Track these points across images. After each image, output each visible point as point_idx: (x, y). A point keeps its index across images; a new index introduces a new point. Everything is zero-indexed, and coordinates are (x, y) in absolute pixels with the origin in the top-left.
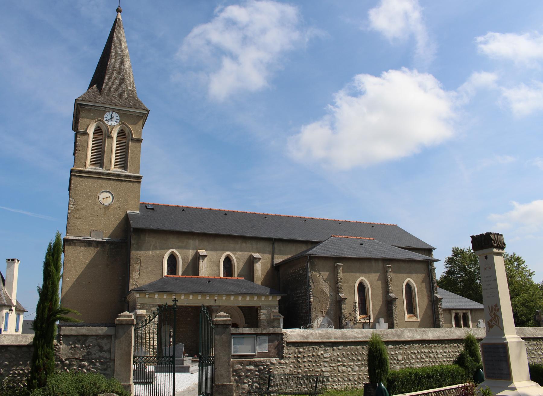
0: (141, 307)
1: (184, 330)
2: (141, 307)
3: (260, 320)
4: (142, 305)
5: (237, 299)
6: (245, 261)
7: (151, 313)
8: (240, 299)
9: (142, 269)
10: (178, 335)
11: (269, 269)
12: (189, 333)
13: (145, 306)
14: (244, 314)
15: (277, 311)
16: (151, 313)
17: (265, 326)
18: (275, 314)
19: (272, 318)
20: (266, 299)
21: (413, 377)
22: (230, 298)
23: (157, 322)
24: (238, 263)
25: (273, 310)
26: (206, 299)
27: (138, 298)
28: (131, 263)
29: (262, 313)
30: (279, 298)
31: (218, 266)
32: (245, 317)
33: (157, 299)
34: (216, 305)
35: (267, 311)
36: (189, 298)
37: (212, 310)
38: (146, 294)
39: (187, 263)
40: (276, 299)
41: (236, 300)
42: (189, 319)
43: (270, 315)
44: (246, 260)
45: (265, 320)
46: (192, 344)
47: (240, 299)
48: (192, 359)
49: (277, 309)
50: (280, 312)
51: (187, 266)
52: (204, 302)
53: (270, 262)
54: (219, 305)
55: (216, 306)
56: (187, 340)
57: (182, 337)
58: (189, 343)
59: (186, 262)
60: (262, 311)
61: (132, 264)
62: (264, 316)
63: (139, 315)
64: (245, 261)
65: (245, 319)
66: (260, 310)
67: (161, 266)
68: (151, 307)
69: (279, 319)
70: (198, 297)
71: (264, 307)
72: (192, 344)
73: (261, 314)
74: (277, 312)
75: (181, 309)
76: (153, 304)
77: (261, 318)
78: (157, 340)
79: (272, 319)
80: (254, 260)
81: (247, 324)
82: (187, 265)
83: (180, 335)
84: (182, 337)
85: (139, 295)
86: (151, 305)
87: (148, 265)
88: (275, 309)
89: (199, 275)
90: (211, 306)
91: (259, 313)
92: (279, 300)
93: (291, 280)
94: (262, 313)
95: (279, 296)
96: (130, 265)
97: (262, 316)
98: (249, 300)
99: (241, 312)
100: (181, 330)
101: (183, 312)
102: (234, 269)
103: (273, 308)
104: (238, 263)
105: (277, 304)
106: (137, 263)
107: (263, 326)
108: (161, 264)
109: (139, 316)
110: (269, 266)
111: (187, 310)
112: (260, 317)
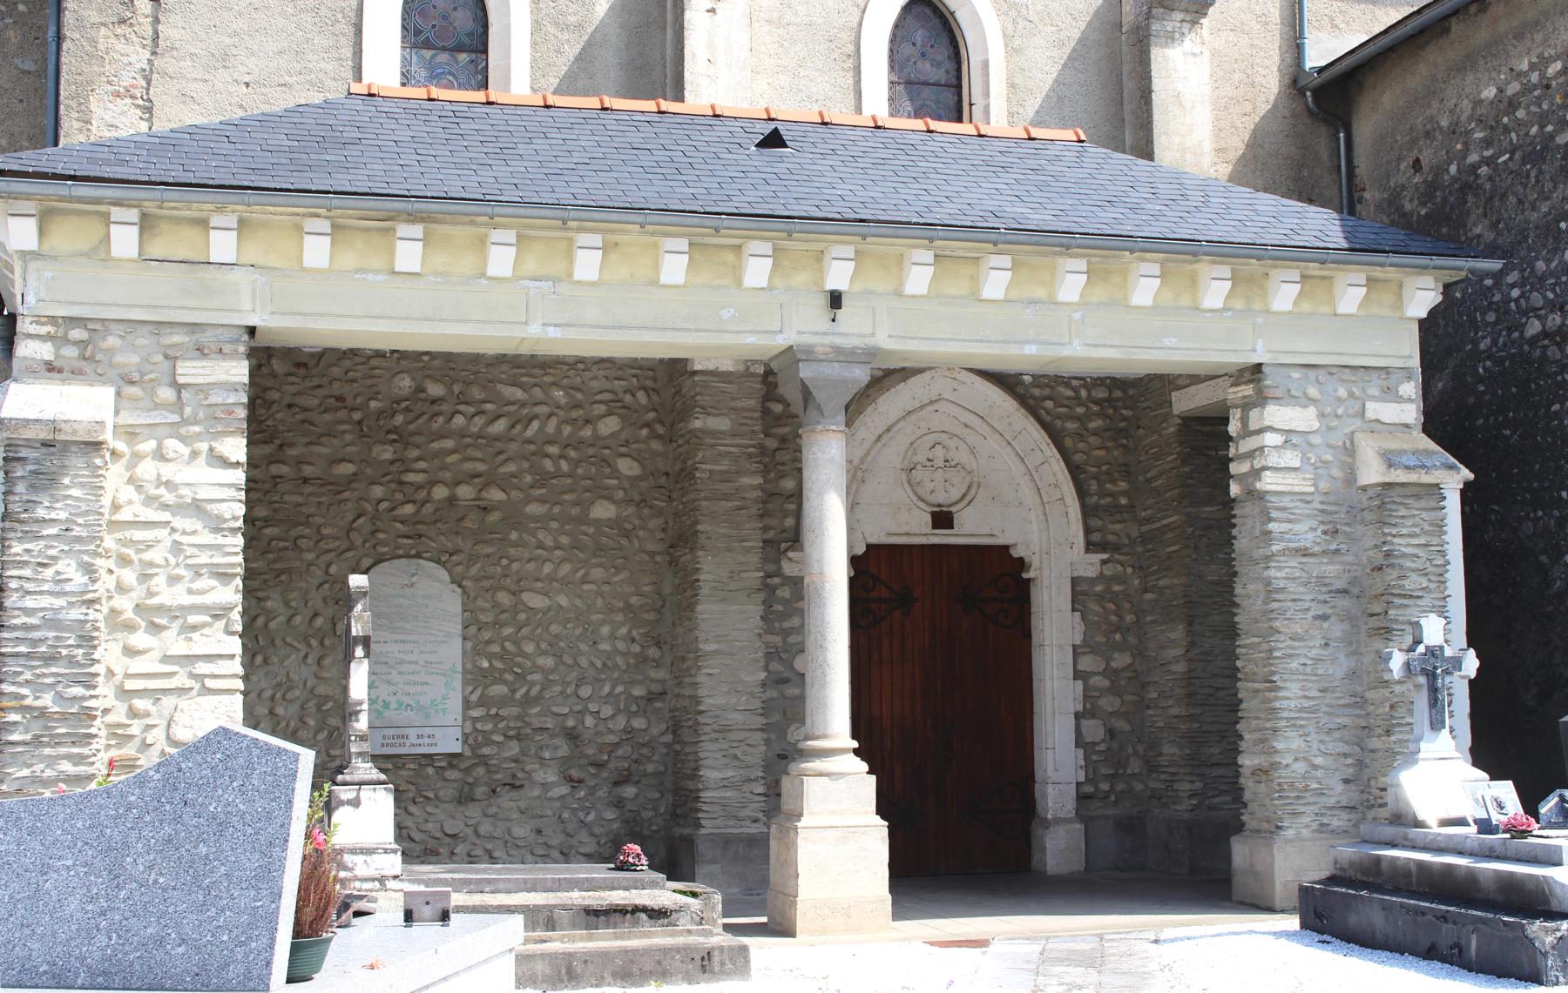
0: (71, 352)
1: (563, 601)
2: (71, 352)
3: (1253, 495)
4: (77, 334)
5: (1040, 293)
6: (1074, 31)
7: (175, 418)
8: (1075, 298)
9: (170, 70)
10: (508, 645)
11: (1264, 108)
12: (605, 630)
13: (112, 341)
14: (1074, 470)
15: (1411, 413)
16: (175, 418)
17: (1305, 552)
18: (1394, 445)
19: (1372, 472)
20: (1306, 307)
21: (498, 690)
22: (976, 281)
23: (240, 510)
24: (1016, 51)
25: (1370, 405)
26: (739, 282)
27: (33, 266)
28: (68, 18)
29: (1270, 429)
30: (1422, 297)
31: (849, 64)
32: (1081, 493)
33: (237, 275)
34: (838, 341)
35: (1321, 415)
36: (570, 274)
37: (807, 394)
38: (117, 213)
39: (580, 26)
40: (1399, 303)
41: (1032, 302)
42: (603, 510)
43: (1350, 450)
44: (1083, 26)
45: (1303, 498)
46: (639, 723)
47: (1075, 298)
48: (527, 941)
49: (1410, 400)
50: (1434, 424)
51: (579, 58)
52: (726, 314)
53: (1277, 59)
54: (871, 342)
55: (838, 350)
56: (585, 692)
57: (548, 662)
58: (607, 711)
59: (572, 19)
60: (1276, 415)
61: (80, 24)
62: (1291, 459)
63: (29, 434)
64: (1077, 34)
65: (1087, 512)
66: (1261, 399)
67: (347, 52)
68: (172, 359)
69: (1437, 486)
70: (657, 265)
71: (1296, 375)
72: (639, 723)
73: (1271, 439)
74: (1407, 426)
75: (535, 424)
76: (194, 327)
77: (1269, 482)
78: (245, 693)
79: (1364, 489)
80: (1149, 16)
81: (1097, 558)
82: (577, 49)
83: (529, 648)
84: (548, 662)
85: (31, 224)
86: (178, 338)
87: (228, 41)
88: (1390, 394)
89: (679, 97)
90: (791, 355)
91: (1247, 433)
92: (1424, 315)
93: (1484, 170)
94: (1270, 429)
95: (1428, 281)
96: (59, 38)
97: (1272, 459)
98: (1155, 308)
99: (1051, 452)
100: (535, 601)
101: (553, 450)
102: (987, 95)
103: (1374, 391)
104: (1012, 51)
105: (1407, 351)
106: (122, 21)
107: (1283, 552)
108: (350, 31)
109: (29, 443)
110: (1270, 83)
111: (587, 432)
112: (1257, 473)
